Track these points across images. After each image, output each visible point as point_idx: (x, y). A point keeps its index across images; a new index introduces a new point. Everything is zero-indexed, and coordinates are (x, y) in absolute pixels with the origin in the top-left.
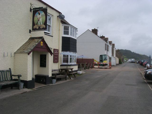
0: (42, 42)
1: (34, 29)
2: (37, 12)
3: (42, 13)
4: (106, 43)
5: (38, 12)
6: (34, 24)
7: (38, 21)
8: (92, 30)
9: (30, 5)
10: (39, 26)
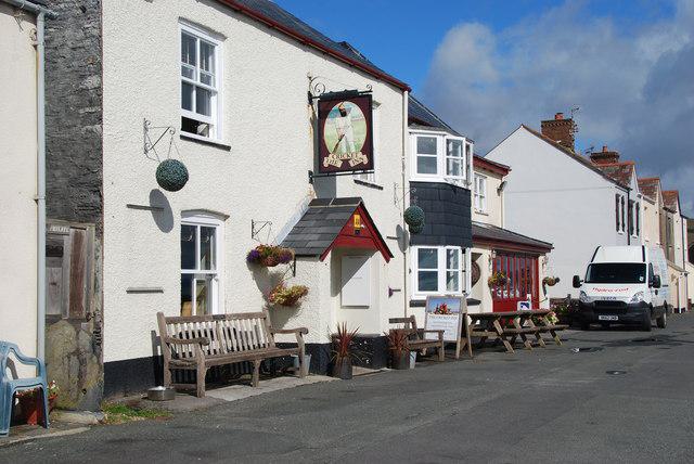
0: (357, 217)
3: (355, 110)
4: (623, 193)
8: (545, 124)
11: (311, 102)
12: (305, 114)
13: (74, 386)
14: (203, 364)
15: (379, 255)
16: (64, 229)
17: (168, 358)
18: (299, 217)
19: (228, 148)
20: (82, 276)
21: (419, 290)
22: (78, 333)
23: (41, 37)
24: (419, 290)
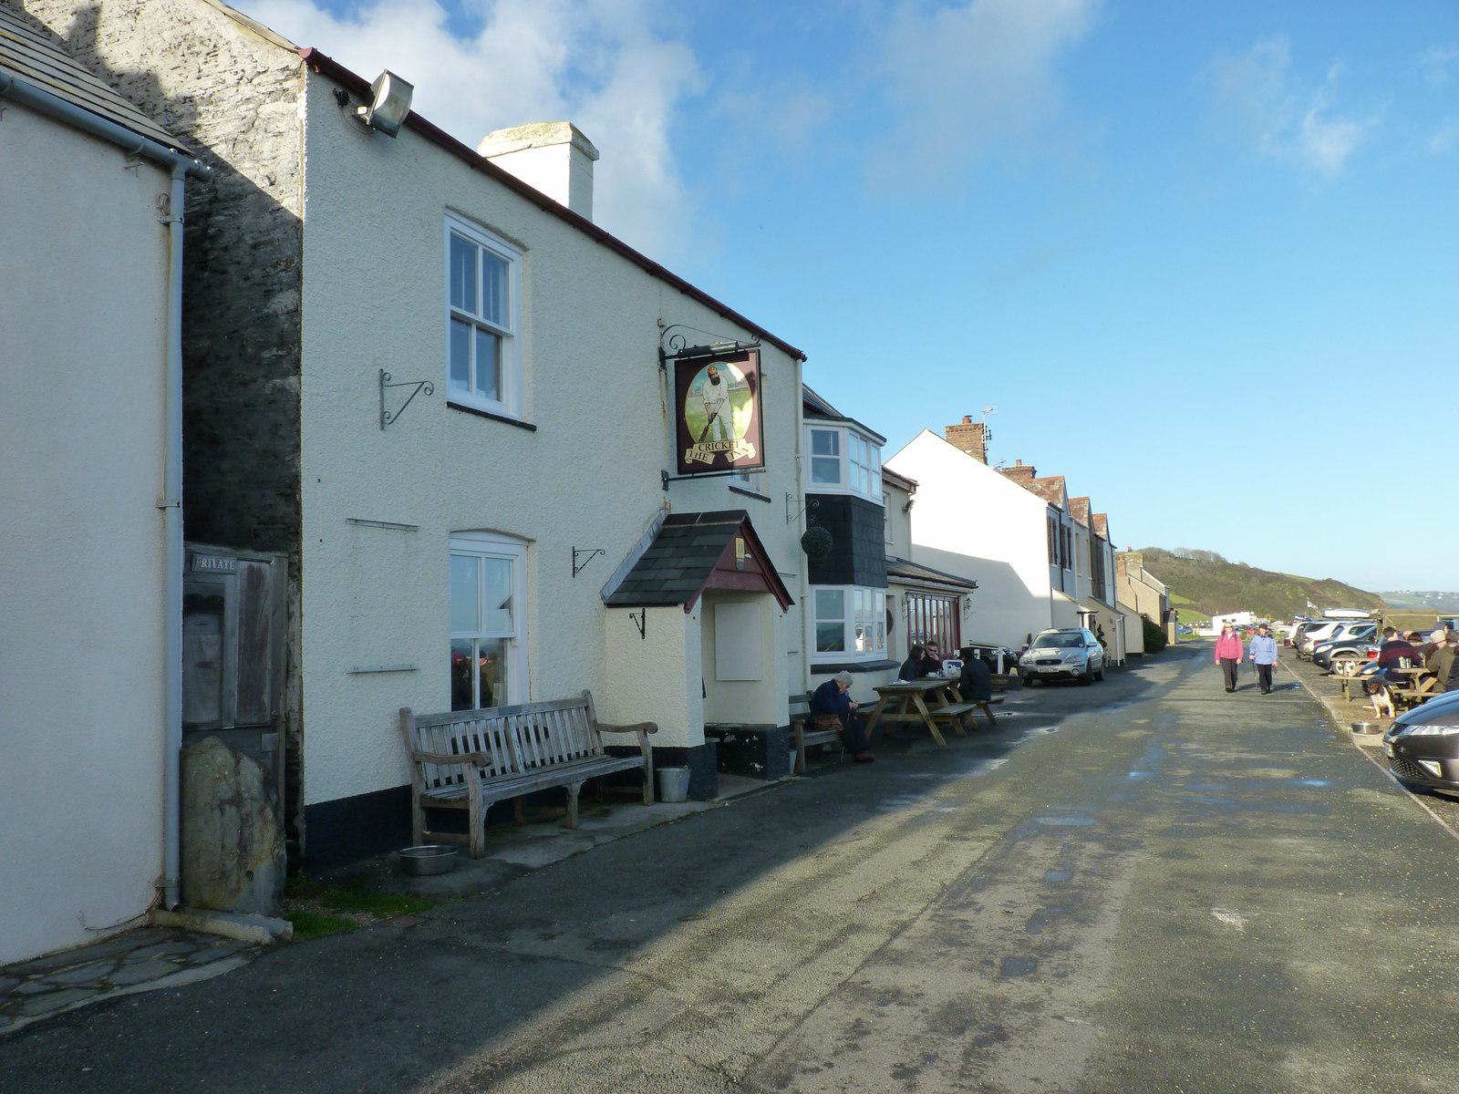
0: (740, 542)
1: (689, 470)
2: (704, 371)
5: (708, 367)
6: (683, 439)
7: (711, 421)
9: (658, 331)
10: (720, 447)
11: (663, 366)
12: (652, 388)
13: (231, 863)
14: (479, 799)
15: (772, 600)
16: (226, 563)
17: (419, 790)
18: (648, 543)
19: (532, 428)
20: (263, 646)
21: (818, 651)
22: (238, 763)
23: (177, 209)
24: (818, 651)
